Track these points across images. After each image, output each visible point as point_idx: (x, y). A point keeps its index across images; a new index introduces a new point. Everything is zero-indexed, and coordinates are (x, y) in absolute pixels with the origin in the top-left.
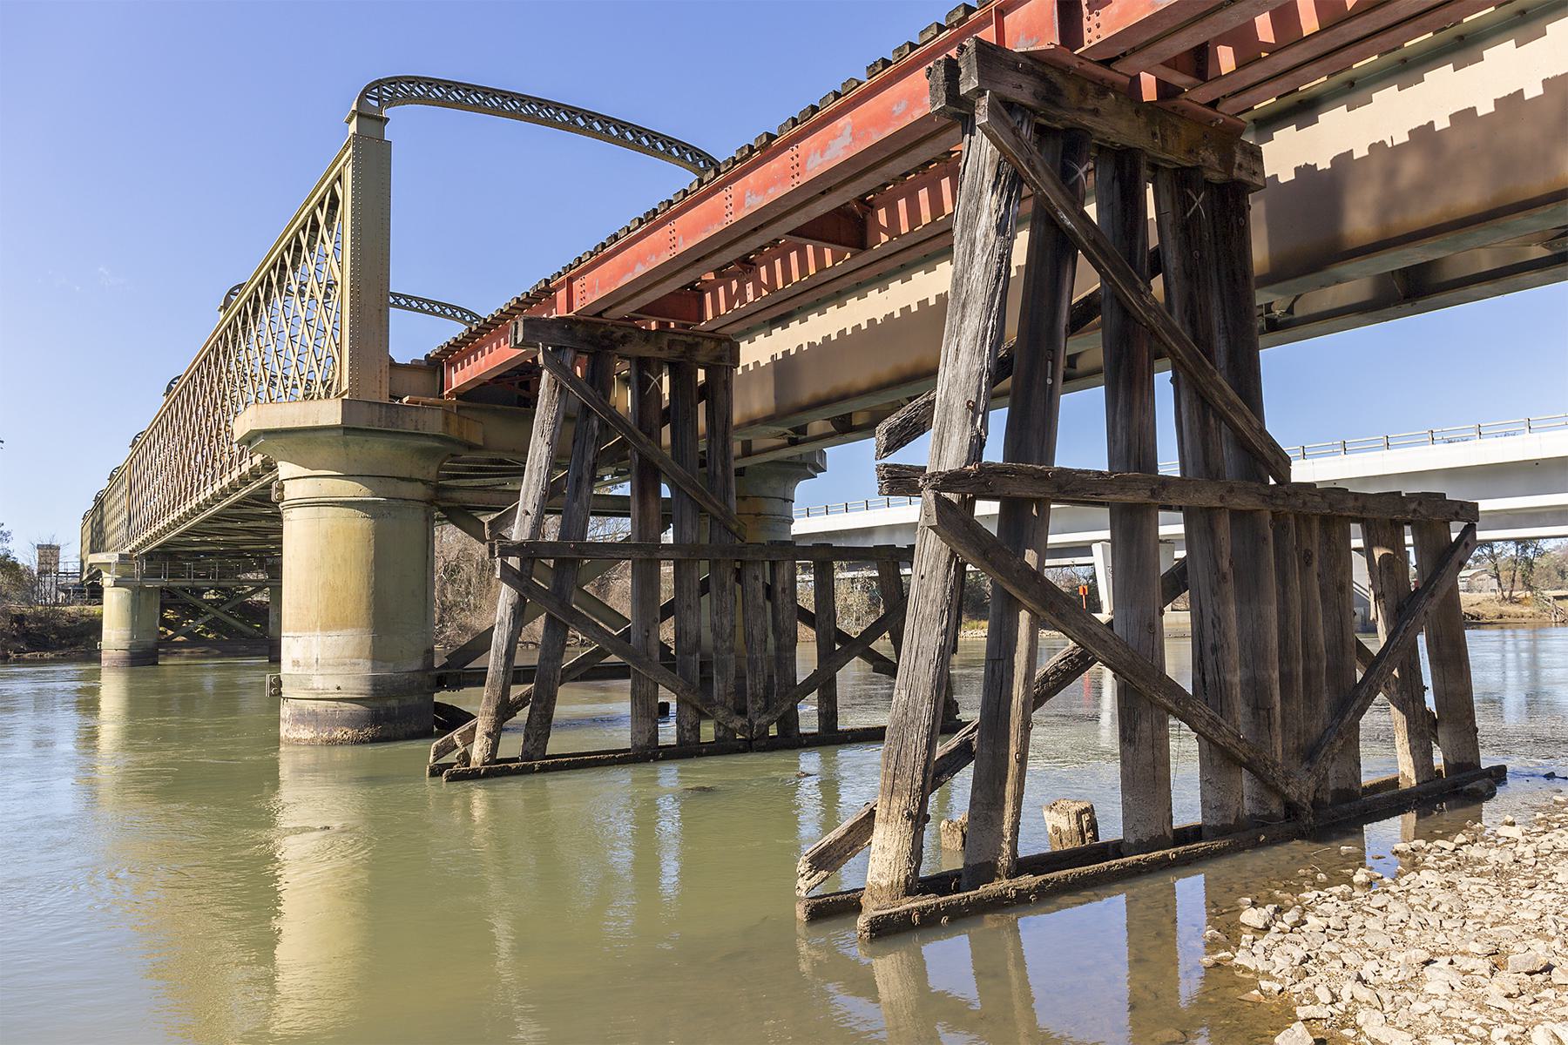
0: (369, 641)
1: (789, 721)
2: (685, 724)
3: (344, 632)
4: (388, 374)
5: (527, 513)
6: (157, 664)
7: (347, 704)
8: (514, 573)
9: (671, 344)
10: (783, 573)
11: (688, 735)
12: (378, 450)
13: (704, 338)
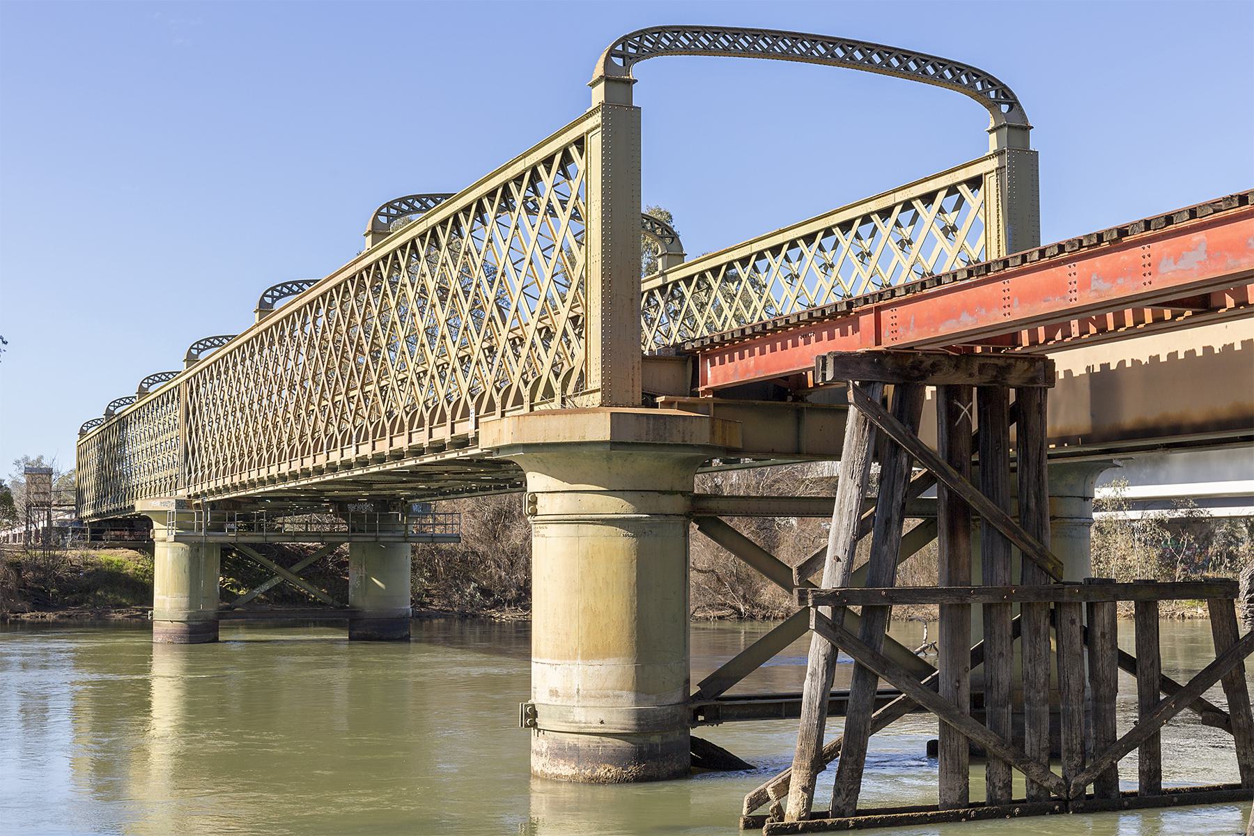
0: (632, 671)
1: (1108, 779)
2: (997, 781)
3: (612, 661)
4: (640, 371)
5: (838, 560)
6: (216, 640)
7: (610, 740)
8: (828, 624)
9: (982, 368)
10: (1102, 616)
11: (999, 793)
12: (643, 464)
13: (1017, 359)
